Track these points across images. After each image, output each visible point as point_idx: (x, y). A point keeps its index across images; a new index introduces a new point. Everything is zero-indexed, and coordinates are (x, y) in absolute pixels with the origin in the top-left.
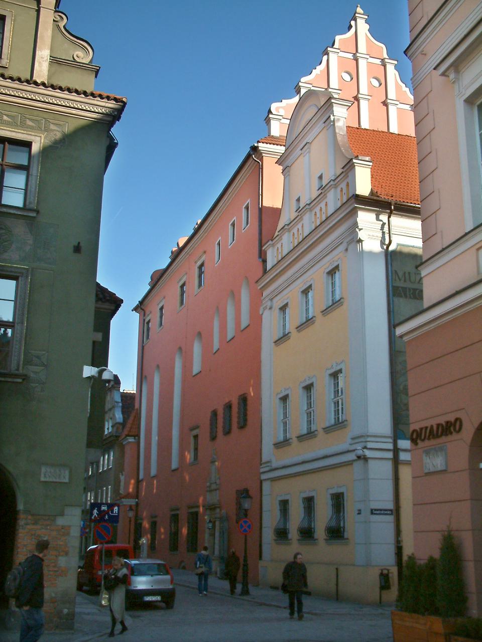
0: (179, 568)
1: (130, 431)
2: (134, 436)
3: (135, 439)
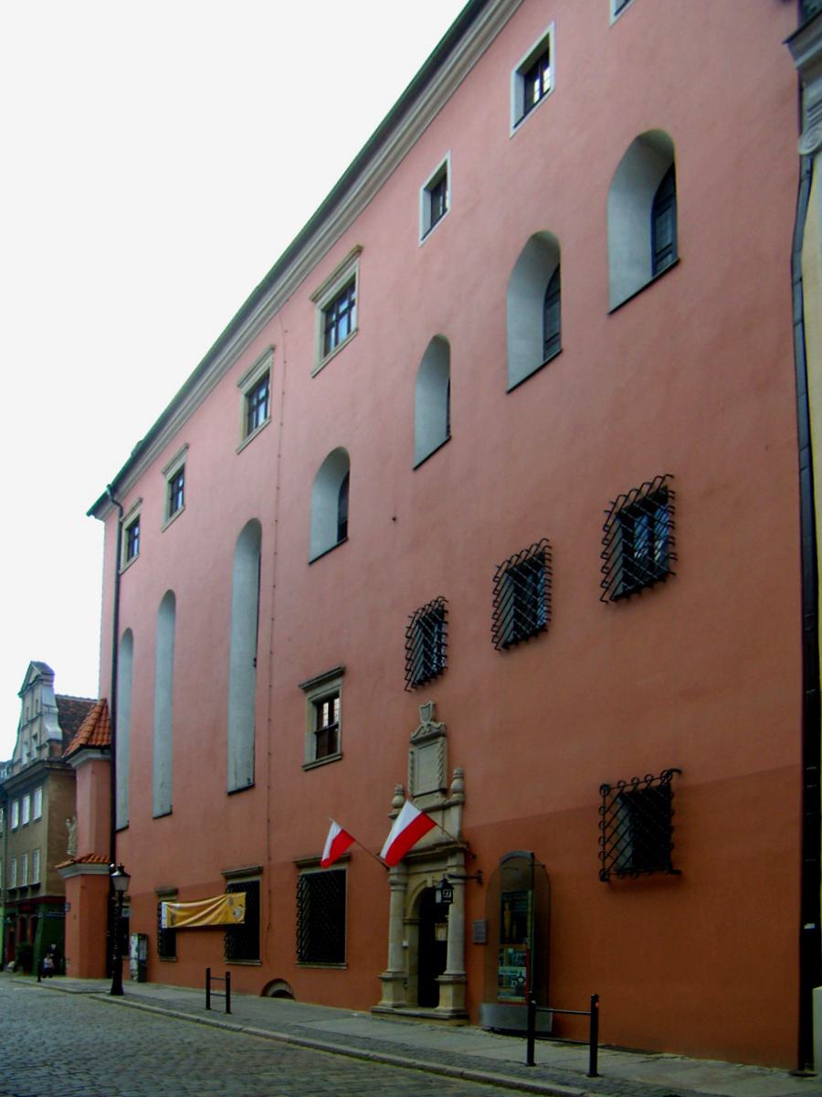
0: (264, 993)
1: (89, 739)
2: (102, 749)
3: (102, 753)
